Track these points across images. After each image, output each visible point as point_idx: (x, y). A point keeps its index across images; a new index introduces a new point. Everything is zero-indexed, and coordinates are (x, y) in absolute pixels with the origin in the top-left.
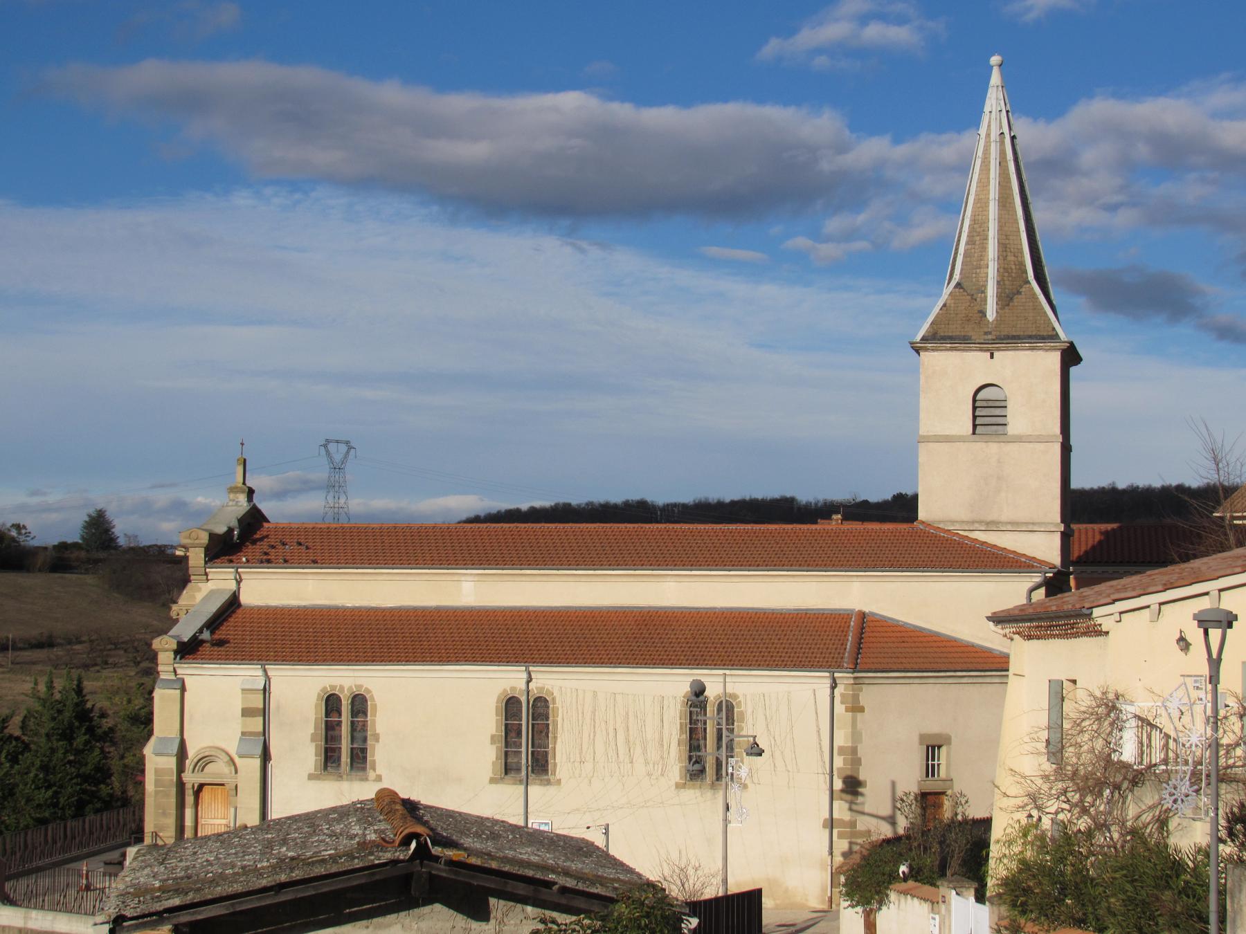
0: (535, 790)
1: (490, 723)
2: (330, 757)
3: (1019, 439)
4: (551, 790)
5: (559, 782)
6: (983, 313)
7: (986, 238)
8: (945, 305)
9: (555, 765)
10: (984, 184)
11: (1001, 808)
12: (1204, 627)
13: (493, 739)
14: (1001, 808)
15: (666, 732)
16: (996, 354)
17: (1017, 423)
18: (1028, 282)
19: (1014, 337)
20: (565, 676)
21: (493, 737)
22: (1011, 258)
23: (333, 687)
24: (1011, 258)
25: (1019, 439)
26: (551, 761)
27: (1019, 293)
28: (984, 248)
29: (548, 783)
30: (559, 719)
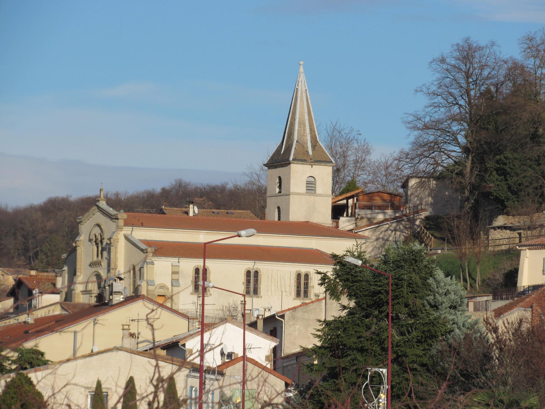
0: (255, 299)
1: (242, 278)
2: (298, 294)
3: (320, 195)
4: (259, 299)
5: (261, 297)
6: (308, 152)
7: (305, 126)
8: (295, 148)
9: (260, 292)
10: (302, 108)
11: (121, 279)
12: (187, 216)
13: (243, 283)
14: (121, 279)
15: (291, 284)
16: (313, 166)
17: (319, 190)
18: (318, 142)
19: (319, 161)
20: (268, 265)
21: (243, 283)
22: (313, 133)
23: (198, 266)
24: (313, 133)
25: (320, 195)
26: (259, 290)
27: (316, 146)
28: (305, 130)
29: (258, 297)
30: (262, 278)
